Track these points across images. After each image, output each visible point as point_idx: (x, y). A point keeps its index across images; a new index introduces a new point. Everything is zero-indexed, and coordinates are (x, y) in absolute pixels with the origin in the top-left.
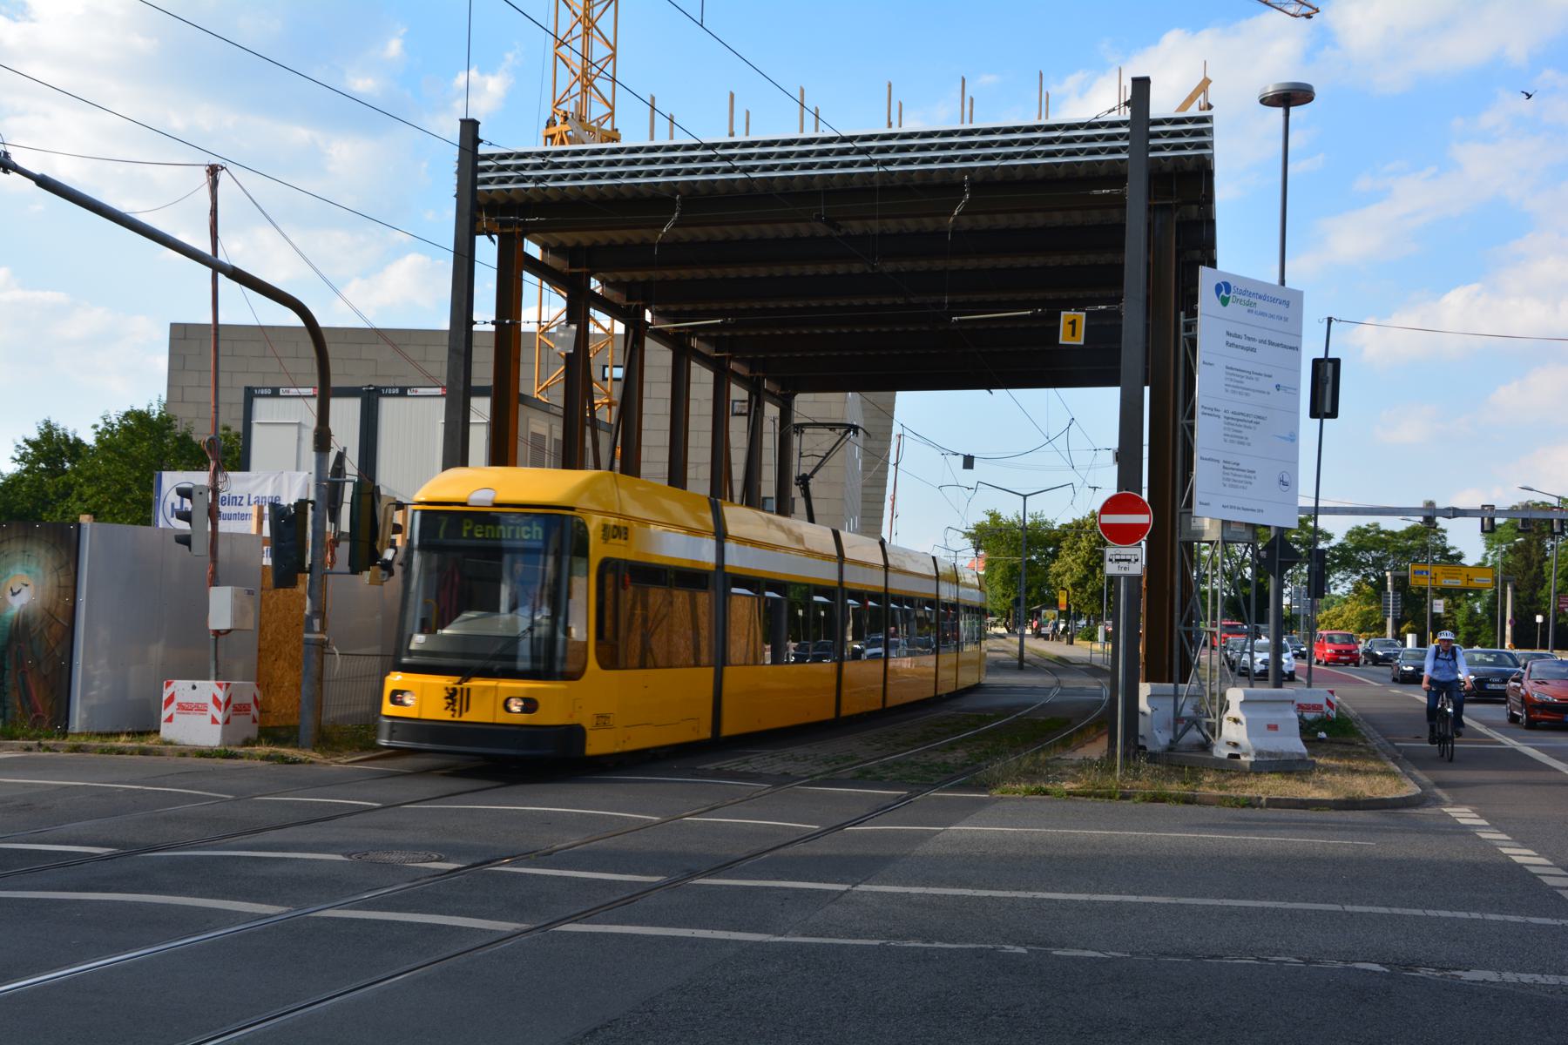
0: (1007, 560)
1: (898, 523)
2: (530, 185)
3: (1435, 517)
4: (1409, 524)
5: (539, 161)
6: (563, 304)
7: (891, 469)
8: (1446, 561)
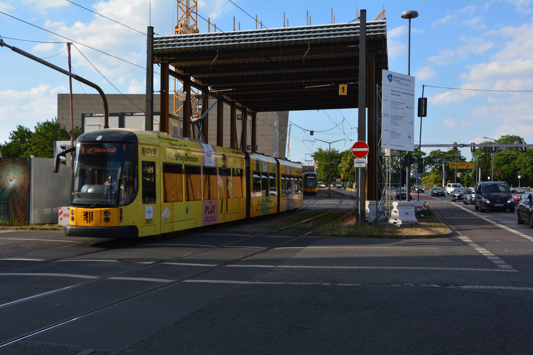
1: (290, 153)
7: (288, 136)
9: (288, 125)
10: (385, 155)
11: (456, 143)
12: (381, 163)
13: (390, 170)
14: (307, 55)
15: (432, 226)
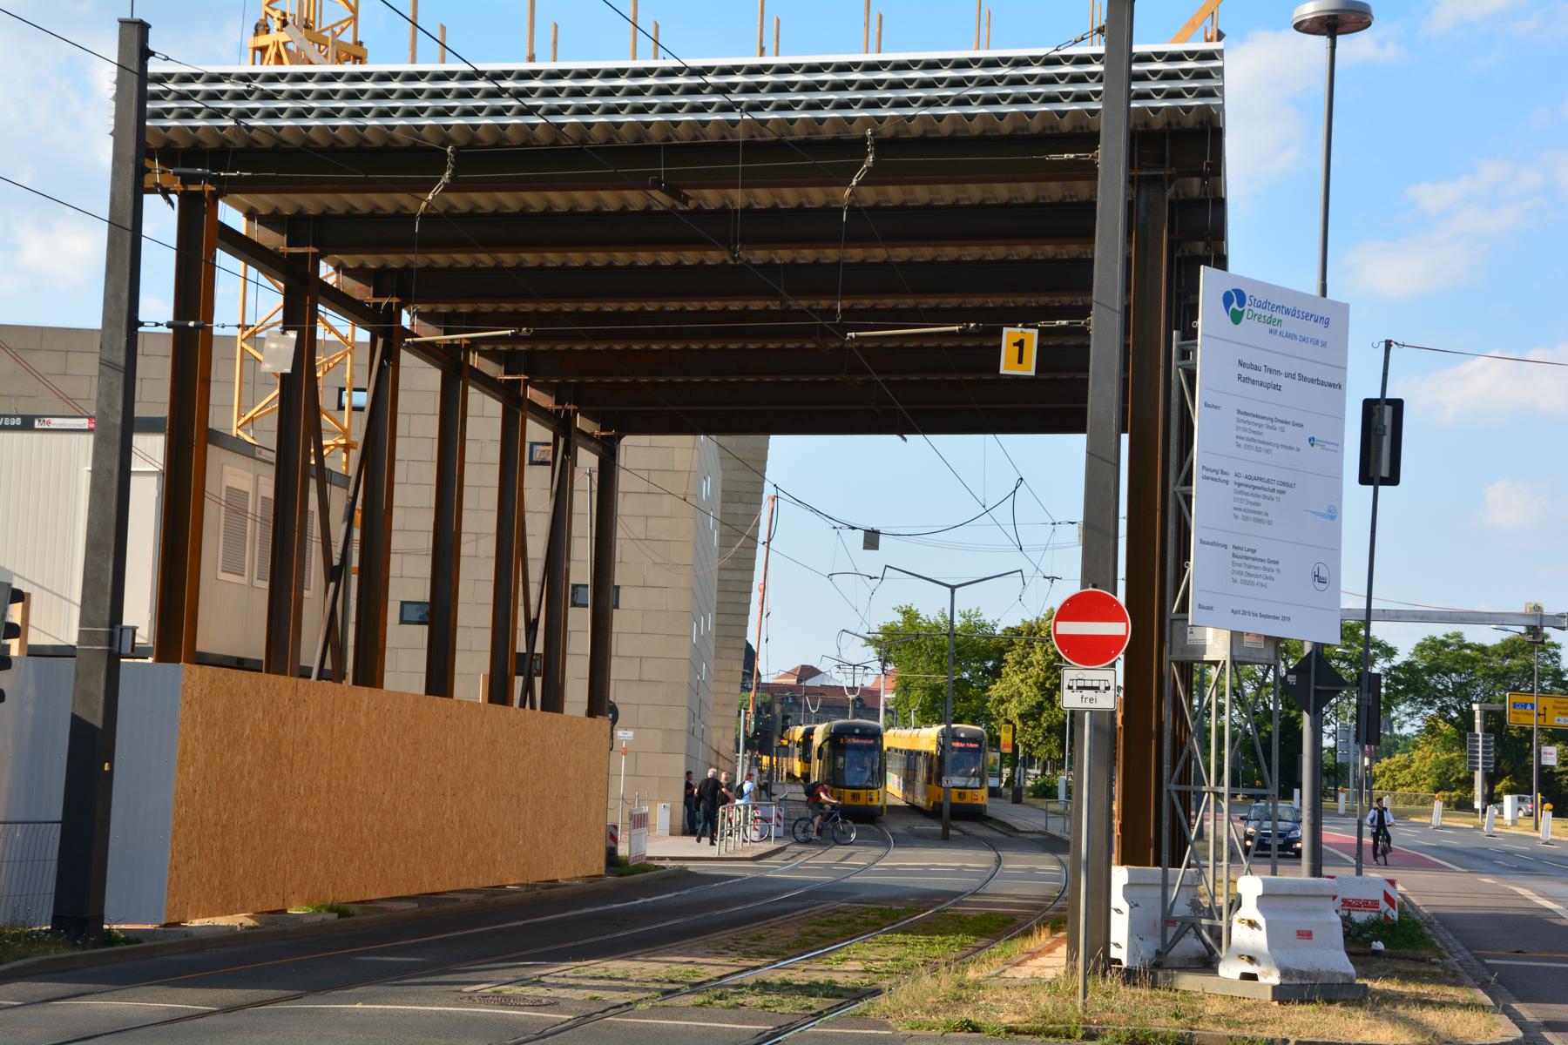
0: (926, 679)
1: (771, 627)
2: (228, 122)
3: (1542, 627)
4: (1506, 635)
5: (242, 87)
6: (279, 300)
7: (761, 551)
8: (1562, 690)
9: (765, 496)
10: (1206, 658)
11: (1538, 608)
12: (1186, 694)
13: (1226, 718)
14: (863, 189)
15: (1424, 1002)
